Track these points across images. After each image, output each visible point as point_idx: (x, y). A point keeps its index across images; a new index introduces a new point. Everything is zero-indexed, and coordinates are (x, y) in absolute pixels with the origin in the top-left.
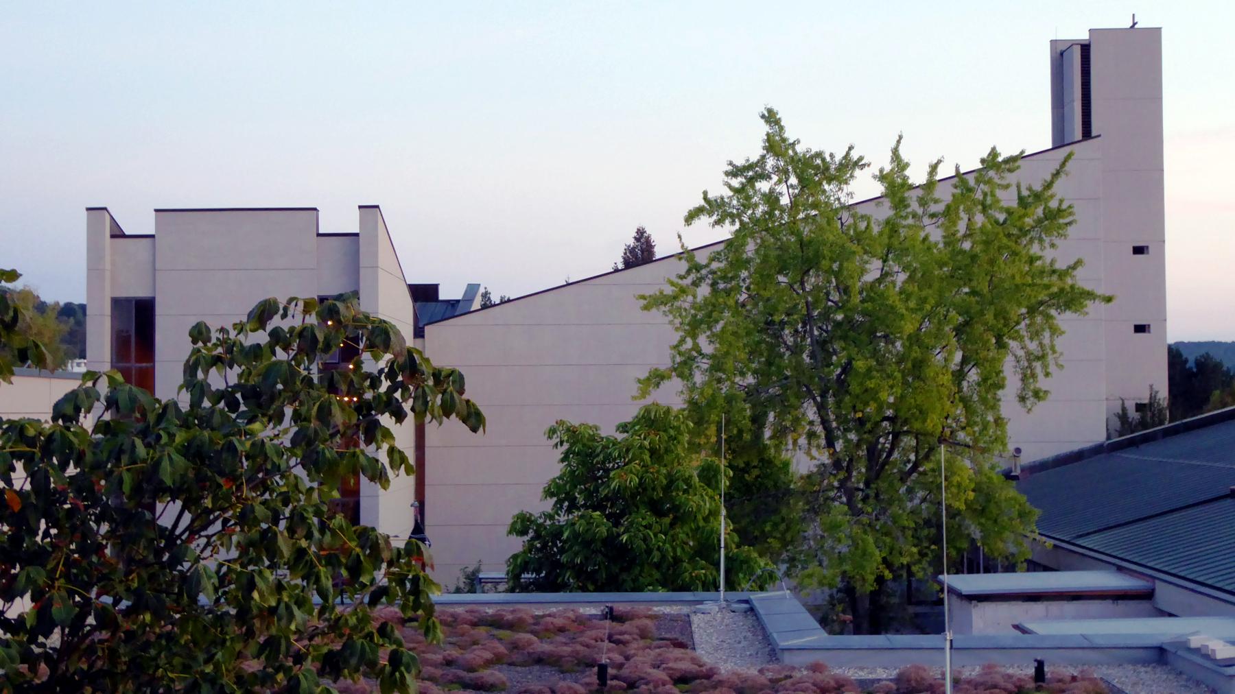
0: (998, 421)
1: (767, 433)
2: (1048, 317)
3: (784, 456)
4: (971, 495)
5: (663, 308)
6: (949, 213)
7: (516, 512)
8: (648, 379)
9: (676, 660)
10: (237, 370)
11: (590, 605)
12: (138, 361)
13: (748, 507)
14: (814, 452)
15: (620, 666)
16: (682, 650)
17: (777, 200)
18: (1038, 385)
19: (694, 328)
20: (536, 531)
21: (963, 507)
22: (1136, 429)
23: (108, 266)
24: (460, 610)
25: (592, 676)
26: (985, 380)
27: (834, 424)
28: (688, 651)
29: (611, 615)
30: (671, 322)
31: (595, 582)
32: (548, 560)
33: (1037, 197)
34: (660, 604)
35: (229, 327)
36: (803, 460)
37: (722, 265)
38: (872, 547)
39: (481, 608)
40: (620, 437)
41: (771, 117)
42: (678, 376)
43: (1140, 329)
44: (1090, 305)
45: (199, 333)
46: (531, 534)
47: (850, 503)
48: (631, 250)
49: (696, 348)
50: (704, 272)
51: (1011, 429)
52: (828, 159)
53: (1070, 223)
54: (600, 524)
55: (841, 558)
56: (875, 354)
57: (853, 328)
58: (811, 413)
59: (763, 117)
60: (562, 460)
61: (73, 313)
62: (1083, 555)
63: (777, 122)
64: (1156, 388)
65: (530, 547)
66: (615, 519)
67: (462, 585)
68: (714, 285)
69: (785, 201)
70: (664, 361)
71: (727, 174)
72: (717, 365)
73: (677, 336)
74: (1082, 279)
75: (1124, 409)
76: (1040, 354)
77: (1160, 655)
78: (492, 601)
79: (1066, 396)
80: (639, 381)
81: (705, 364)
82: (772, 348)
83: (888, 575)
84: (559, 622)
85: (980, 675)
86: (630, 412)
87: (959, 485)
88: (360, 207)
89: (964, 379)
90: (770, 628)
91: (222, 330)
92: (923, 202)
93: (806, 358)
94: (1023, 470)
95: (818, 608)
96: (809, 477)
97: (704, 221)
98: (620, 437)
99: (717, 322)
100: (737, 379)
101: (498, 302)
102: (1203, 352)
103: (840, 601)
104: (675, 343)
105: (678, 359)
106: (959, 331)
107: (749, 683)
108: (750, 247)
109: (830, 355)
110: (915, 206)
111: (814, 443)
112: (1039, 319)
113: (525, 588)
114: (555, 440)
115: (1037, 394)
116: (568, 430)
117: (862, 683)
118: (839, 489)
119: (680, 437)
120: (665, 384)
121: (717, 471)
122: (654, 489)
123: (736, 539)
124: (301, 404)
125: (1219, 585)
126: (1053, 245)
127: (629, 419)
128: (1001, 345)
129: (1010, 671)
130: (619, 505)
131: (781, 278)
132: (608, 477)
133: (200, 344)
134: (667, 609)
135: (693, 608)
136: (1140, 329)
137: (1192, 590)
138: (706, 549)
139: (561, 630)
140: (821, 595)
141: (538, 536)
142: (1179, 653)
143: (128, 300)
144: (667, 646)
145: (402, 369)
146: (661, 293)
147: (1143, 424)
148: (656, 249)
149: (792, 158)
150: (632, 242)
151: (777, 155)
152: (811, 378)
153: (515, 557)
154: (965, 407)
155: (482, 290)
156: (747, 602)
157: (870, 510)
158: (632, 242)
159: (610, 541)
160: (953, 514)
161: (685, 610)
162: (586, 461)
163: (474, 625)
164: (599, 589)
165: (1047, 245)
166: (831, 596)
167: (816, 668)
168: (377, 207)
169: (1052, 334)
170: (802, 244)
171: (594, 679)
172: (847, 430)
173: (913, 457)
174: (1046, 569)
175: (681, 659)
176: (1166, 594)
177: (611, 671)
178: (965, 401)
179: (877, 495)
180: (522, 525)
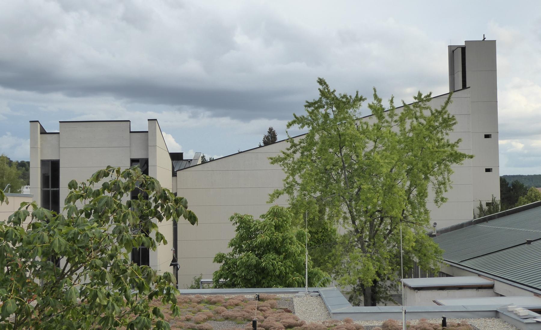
0: (426, 212)
1: (326, 217)
2: (446, 166)
3: (334, 227)
4: (414, 244)
5: (279, 163)
6: (402, 120)
7: (218, 253)
8: (274, 194)
9: (287, 318)
10: (89, 200)
11: (250, 294)
12: (52, 188)
13: (318, 249)
14: (346, 226)
15: (262, 321)
16: (289, 314)
17: (328, 116)
18: (443, 196)
19: (293, 172)
20: (225, 261)
21: (411, 249)
22: (488, 214)
23: (39, 146)
24: (193, 296)
25: (250, 325)
26: (419, 194)
27: (355, 213)
28: (292, 314)
29: (259, 299)
30: (283, 169)
31: (251, 284)
32: (232, 275)
33: (440, 113)
34: (279, 293)
35: (85, 182)
36: (342, 229)
37: (305, 145)
38: (372, 268)
39: (199, 295)
40: (262, 220)
41: (321, 82)
42: (287, 193)
43: (488, 170)
44: (466, 161)
45: (72, 185)
46: (224, 262)
47: (362, 248)
48: (267, 137)
49: (294, 180)
50: (298, 147)
51: (431, 215)
52: (349, 98)
53: (455, 123)
54: (254, 259)
55: (359, 272)
56: (373, 183)
57: (363, 171)
58: (345, 208)
59: (318, 82)
60: (237, 231)
61: (24, 166)
62: (463, 269)
63: (325, 83)
64: (495, 196)
65: (223, 269)
66: (260, 256)
67: (194, 284)
68: (302, 153)
69: (332, 116)
70: (281, 186)
71: (306, 106)
72: (303, 189)
73: (287, 175)
74: (460, 149)
75: (481, 205)
76: (443, 182)
77: (496, 314)
78: (207, 292)
79: (456, 199)
80: (270, 195)
81: (298, 188)
82: (328, 180)
83: (378, 279)
84: (236, 301)
85: (419, 324)
86: (266, 209)
87: (409, 240)
88: (149, 120)
89: (410, 193)
90: (327, 304)
91: (83, 183)
92: (391, 116)
93: (342, 184)
94: (437, 232)
95: (348, 293)
96: (344, 236)
97: (296, 127)
98: (262, 220)
99: (303, 169)
100: (313, 194)
101: (209, 160)
102: (515, 179)
103: (358, 290)
104: (285, 178)
105: (287, 186)
106: (408, 172)
107: (319, 328)
108: (317, 137)
109: (353, 183)
110: (387, 118)
111: (346, 221)
112: (443, 166)
113: (221, 287)
114: (234, 222)
115: (442, 199)
116: (238, 217)
117: (367, 327)
118: (357, 241)
119: (288, 220)
120: (281, 197)
121: (303, 235)
122: (276, 243)
123: (312, 263)
124: (117, 214)
125: (521, 282)
126: (447, 134)
127: (265, 213)
128: (426, 178)
129: (431, 322)
130: (263, 249)
131: (331, 150)
132: (256, 237)
133: (73, 190)
134: (282, 296)
135: (294, 295)
136: (488, 170)
137: (510, 285)
138: (299, 269)
139: (237, 305)
140: (349, 288)
141: (226, 263)
142: (504, 313)
143: (48, 161)
144: (283, 312)
145: (160, 197)
146: (279, 157)
147: (490, 212)
148: (277, 137)
149: (333, 98)
150: (267, 134)
151: (327, 98)
152: (345, 193)
153: (216, 272)
154: (412, 206)
155: (202, 155)
156: (317, 292)
157: (371, 251)
158: (267, 134)
159: (257, 265)
160: (407, 252)
161: (291, 295)
162: (246, 229)
163: (199, 303)
164: (254, 286)
165: (444, 134)
166: (354, 288)
167: (347, 321)
168: (156, 120)
169: (448, 173)
170: (340, 136)
171: (251, 327)
172: (360, 216)
173: (389, 228)
174: (448, 275)
175: (289, 318)
176: (499, 287)
177: (258, 323)
178: (411, 203)
179: (374, 244)
180: (220, 258)
